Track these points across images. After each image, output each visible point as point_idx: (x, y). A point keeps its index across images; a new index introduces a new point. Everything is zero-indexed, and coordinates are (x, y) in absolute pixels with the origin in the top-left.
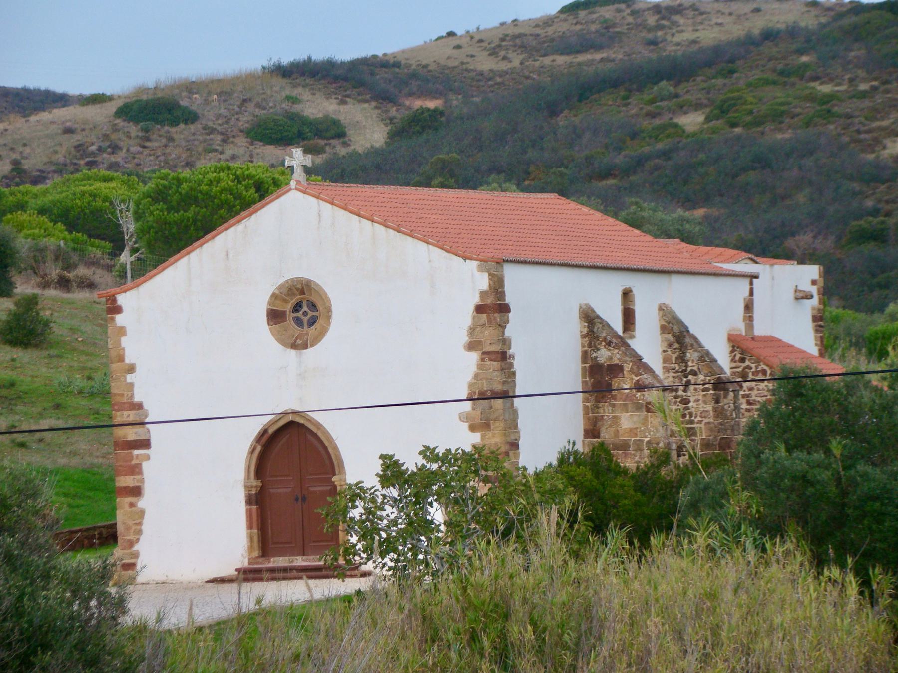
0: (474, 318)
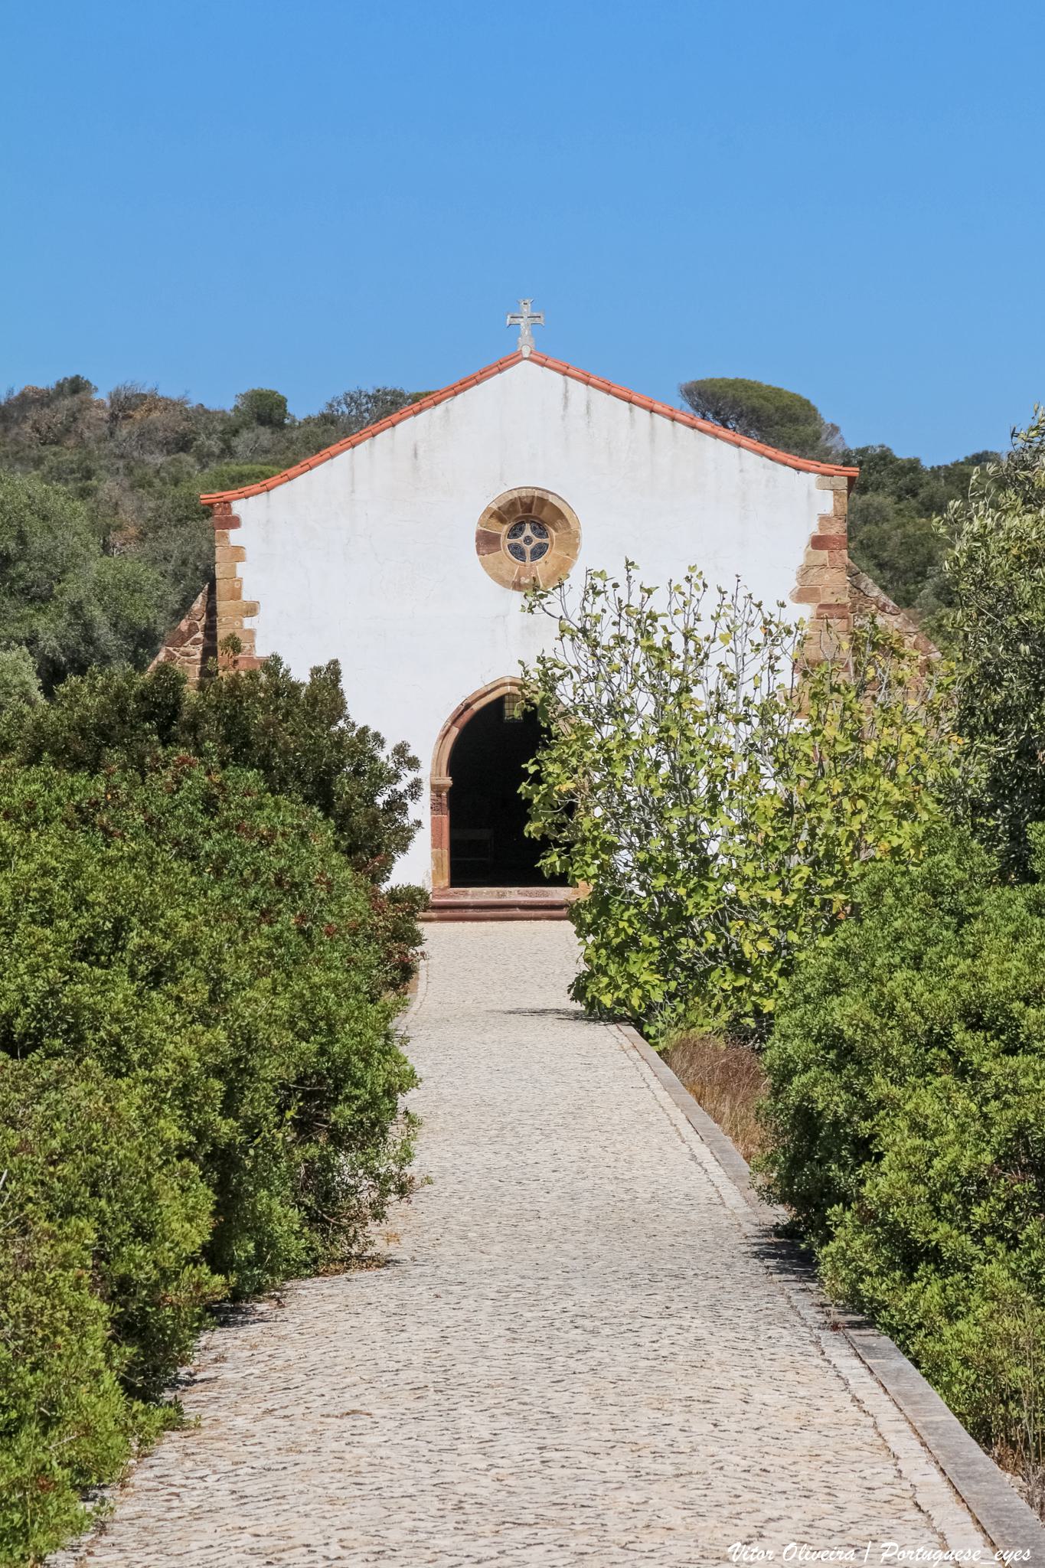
0: (808, 554)
